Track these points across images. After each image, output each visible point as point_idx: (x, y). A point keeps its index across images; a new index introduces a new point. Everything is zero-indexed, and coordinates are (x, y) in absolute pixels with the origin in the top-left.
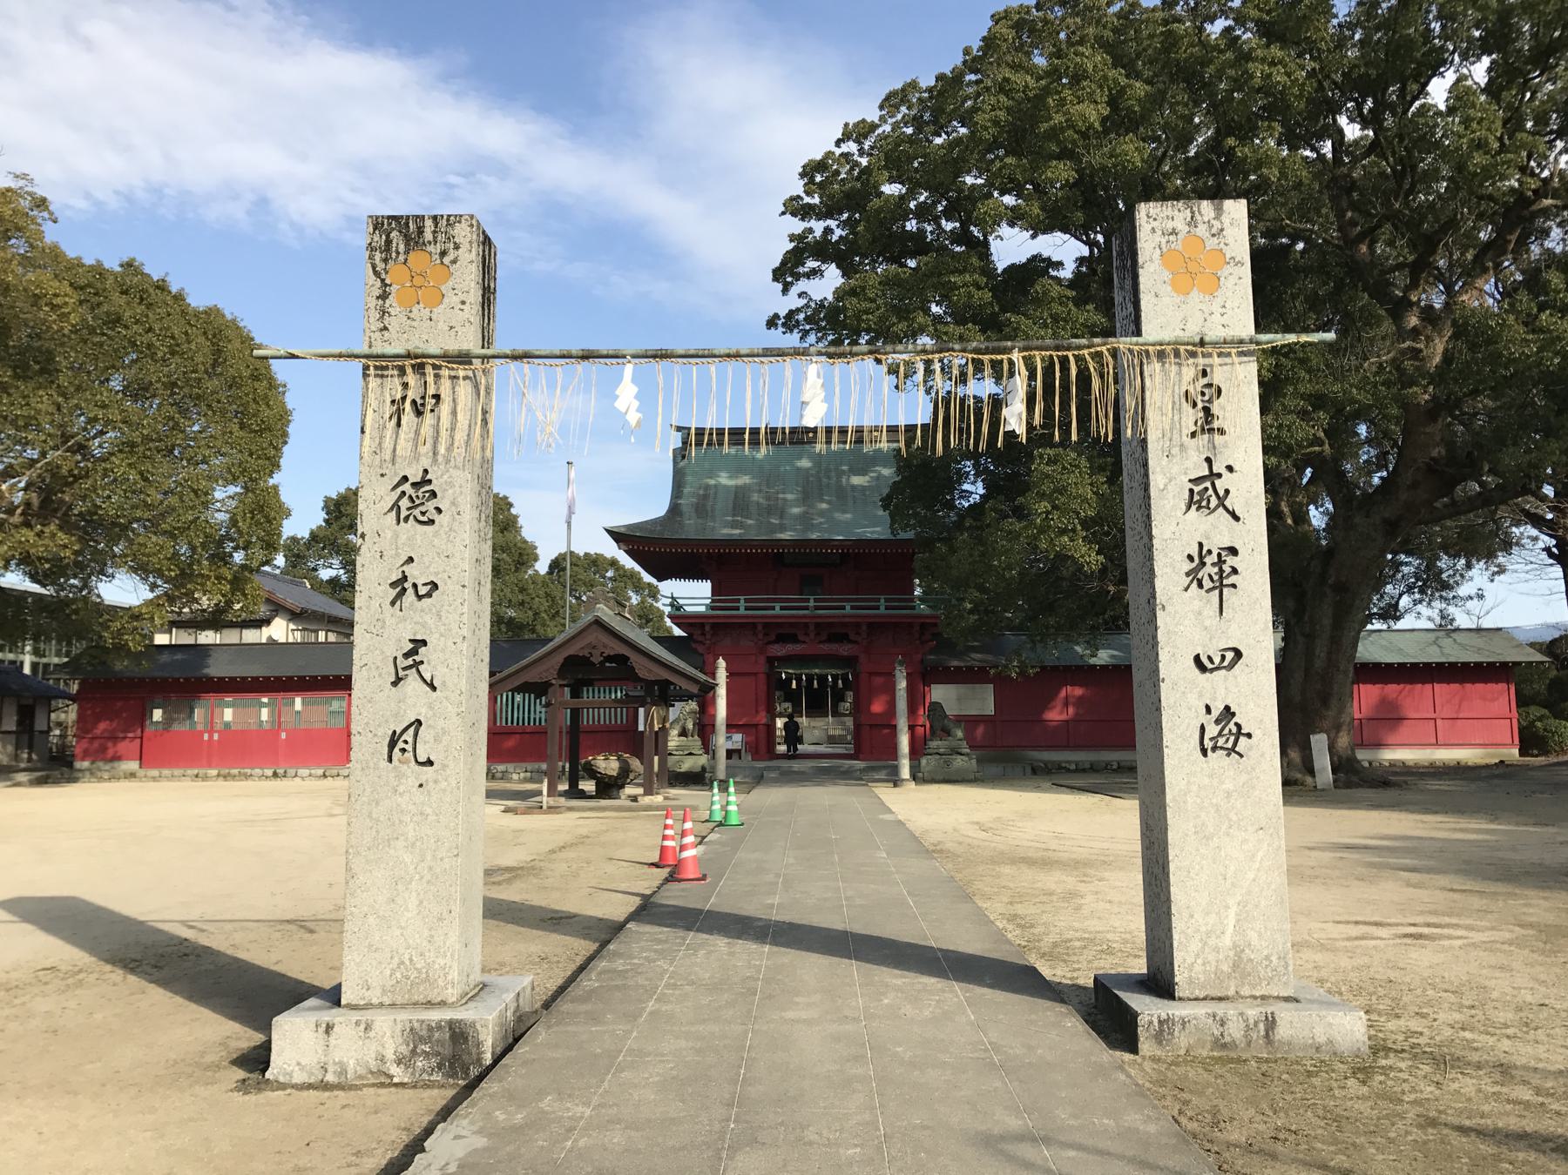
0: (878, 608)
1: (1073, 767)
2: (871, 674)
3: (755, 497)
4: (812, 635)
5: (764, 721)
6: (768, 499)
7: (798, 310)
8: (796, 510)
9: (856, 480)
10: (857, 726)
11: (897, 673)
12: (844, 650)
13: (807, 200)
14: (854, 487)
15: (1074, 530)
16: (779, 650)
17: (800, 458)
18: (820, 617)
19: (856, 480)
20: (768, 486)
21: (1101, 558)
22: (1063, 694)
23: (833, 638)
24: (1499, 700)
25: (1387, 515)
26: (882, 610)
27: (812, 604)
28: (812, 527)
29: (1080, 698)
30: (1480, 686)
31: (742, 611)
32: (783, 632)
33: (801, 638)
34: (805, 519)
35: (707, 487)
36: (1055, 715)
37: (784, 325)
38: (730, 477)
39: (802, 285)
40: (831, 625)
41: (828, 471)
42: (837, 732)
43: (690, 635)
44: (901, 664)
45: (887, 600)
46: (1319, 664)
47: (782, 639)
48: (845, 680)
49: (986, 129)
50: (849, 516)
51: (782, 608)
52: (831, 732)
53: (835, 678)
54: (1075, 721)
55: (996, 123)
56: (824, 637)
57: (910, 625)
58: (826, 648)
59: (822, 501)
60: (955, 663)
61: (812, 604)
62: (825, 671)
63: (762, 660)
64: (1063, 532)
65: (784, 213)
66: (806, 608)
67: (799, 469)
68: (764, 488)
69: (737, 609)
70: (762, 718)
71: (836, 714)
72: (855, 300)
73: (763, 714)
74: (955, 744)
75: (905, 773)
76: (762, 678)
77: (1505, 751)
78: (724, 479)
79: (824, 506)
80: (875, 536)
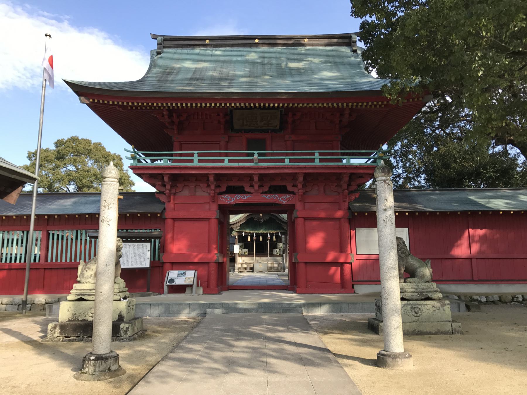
4: (256, 187)
9: (292, 65)
10: (294, 266)
12: (283, 199)
14: (291, 69)
16: (229, 200)
17: (249, 53)
19: (292, 65)
22: (466, 234)
23: (273, 190)
26: (317, 163)
28: (257, 87)
33: (247, 189)
35: (173, 68)
36: (461, 250)
38: (192, 64)
41: (270, 61)
43: (159, 192)
45: (320, 154)
47: (231, 190)
48: (277, 236)
50: (288, 82)
51: (230, 161)
52: (270, 265)
56: (266, 189)
58: (269, 198)
59: (265, 74)
62: (265, 232)
63: (214, 207)
66: (251, 161)
67: (247, 60)
68: (219, 69)
69: (192, 161)
71: (272, 255)
74: (423, 286)
76: (214, 223)
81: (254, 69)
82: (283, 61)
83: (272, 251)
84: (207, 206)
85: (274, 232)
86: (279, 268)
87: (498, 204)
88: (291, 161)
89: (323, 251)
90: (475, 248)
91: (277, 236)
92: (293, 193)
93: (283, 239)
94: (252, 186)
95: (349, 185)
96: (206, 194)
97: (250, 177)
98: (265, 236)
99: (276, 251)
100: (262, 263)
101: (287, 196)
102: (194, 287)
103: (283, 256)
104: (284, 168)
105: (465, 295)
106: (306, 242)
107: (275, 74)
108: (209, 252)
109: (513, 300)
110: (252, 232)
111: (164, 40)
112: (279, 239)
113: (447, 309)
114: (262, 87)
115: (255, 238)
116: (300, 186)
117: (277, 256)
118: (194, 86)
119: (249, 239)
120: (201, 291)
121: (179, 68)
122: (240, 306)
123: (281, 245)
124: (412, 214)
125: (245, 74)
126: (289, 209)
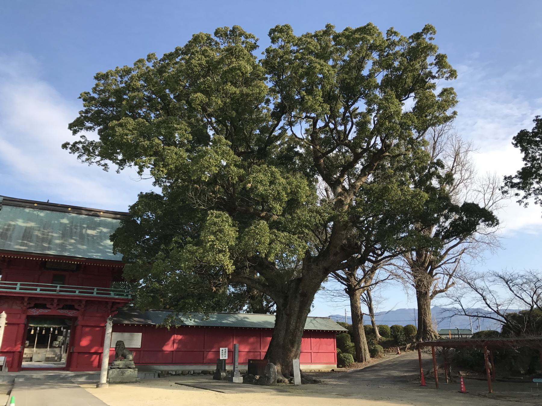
0: (93, 293)
1: (174, 373)
2: (83, 326)
3: (36, 233)
4: (55, 305)
5: (19, 350)
6: (43, 234)
7: (80, 142)
8: (58, 241)
9: (90, 232)
11: (108, 325)
12: (70, 313)
13: (93, 95)
14: (88, 235)
15: (225, 251)
16: (35, 312)
17: (63, 218)
18: (61, 295)
19: (90, 232)
20: (44, 228)
21: (234, 267)
22: (172, 338)
24: (330, 345)
25: (325, 265)
26: (95, 294)
27: (58, 288)
28: (66, 250)
29: (180, 340)
30: (325, 339)
31: (18, 290)
32: (38, 302)
34: (62, 246)
35: (9, 225)
36: (169, 348)
37: (71, 148)
38: (24, 222)
39: (83, 132)
40: (66, 300)
41: (76, 226)
42: (50, 356)
44: (110, 319)
45: (97, 290)
46: (292, 327)
47: (37, 306)
49: (196, 66)
50: (85, 247)
52: (47, 356)
53: (54, 329)
54: (177, 351)
55: (200, 65)
56: (61, 307)
57: (107, 303)
58: (61, 312)
59: (72, 239)
60: (126, 322)
61: (58, 288)
62: (49, 326)
63: (24, 317)
64: (220, 251)
65: (80, 98)
66: (55, 291)
67: (61, 223)
68: (42, 229)
70: (18, 348)
71: (51, 346)
72: (121, 129)
73: (20, 346)
74: (128, 362)
75: (104, 379)
76: (22, 327)
77: (332, 365)
78: (20, 223)
79: (73, 241)
80: (98, 258)
81: (66, 233)
82: (84, 228)
83: (52, 343)
84: (19, 316)
85: (57, 326)
86: (56, 358)
87: (190, 322)
88: (80, 292)
89: (90, 346)
90: (176, 346)
91: (59, 330)
92: (78, 310)
93: (64, 333)
94: (52, 304)
95: (112, 307)
96: (20, 308)
97: (52, 300)
98: (48, 330)
99: (56, 343)
100: (47, 352)
101: (74, 311)
102: (3, 367)
103: (61, 347)
104: (74, 296)
105: (165, 371)
106: (80, 341)
107: (78, 238)
108: (16, 345)
109: (188, 374)
110: (36, 326)
111: (4, 199)
112: (60, 333)
113: (136, 372)
114: (69, 251)
115: (38, 332)
116: (83, 306)
117: (56, 347)
118: (26, 245)
119: (32, 332)
120: (7, 370)
121: (14, 225)
122: (34, 377)
123: (61, 337)
124: (144, 326)
125: (59, 237)
126: (75, 319)
